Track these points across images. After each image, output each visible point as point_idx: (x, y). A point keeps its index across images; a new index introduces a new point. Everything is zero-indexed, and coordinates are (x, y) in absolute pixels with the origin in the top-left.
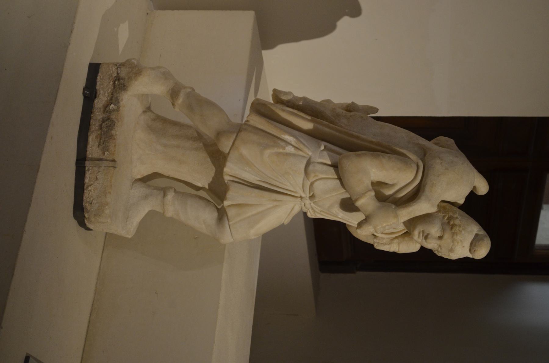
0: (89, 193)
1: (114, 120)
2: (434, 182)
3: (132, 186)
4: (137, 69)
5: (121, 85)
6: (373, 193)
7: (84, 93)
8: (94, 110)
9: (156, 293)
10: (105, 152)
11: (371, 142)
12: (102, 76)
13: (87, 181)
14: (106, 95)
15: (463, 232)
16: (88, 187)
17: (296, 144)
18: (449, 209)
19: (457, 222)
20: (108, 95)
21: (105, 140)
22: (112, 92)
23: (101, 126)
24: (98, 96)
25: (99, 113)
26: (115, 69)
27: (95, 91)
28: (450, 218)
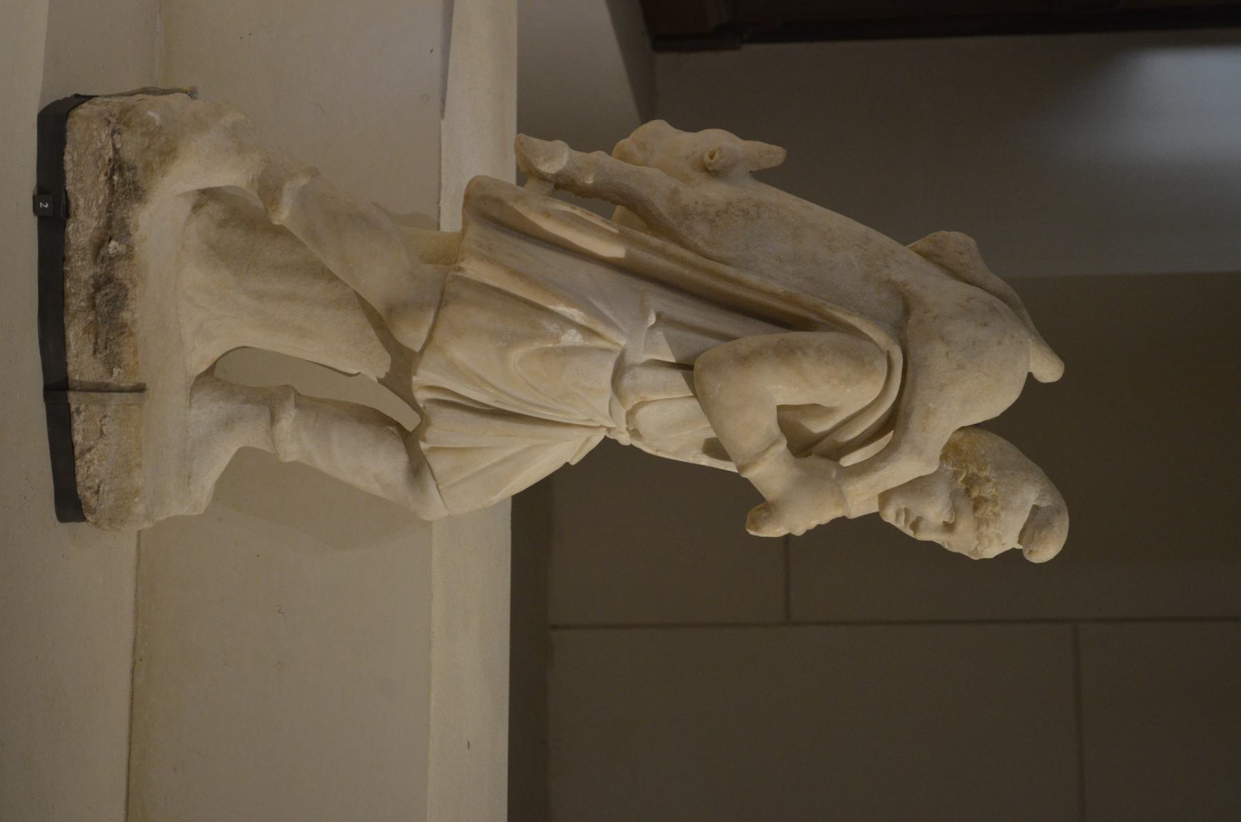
0: (89, 467)
1: (125, 282)
2: (931, 405)
3: (190, 400)
4: (163, 139)
5: (129, 185)
6: (782, 447)
7: (36, 210)
8: (70, 253)
9: (279, 611)
10: (113, 368)
11: (773, 295)
12: (75, 154)
13: (78, 438)
14: (93, 213)
15: (1003, 515)
16: (83, 453)
17: (586, 320)
18: (969, 453)
19: (988, 491)
20: (100, 213)
21: (108, 339)
22: (107, 202)
23: (92, 298)
24: (74, 212)
25: (84, 263)
26: (106, 137)
27: (64, 196)
28: (971, 482)
